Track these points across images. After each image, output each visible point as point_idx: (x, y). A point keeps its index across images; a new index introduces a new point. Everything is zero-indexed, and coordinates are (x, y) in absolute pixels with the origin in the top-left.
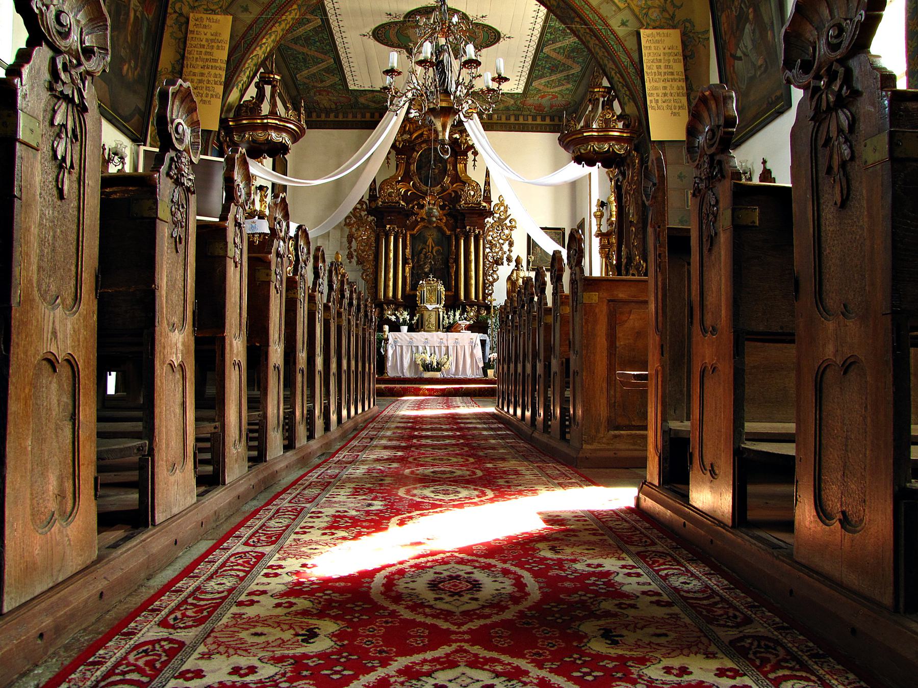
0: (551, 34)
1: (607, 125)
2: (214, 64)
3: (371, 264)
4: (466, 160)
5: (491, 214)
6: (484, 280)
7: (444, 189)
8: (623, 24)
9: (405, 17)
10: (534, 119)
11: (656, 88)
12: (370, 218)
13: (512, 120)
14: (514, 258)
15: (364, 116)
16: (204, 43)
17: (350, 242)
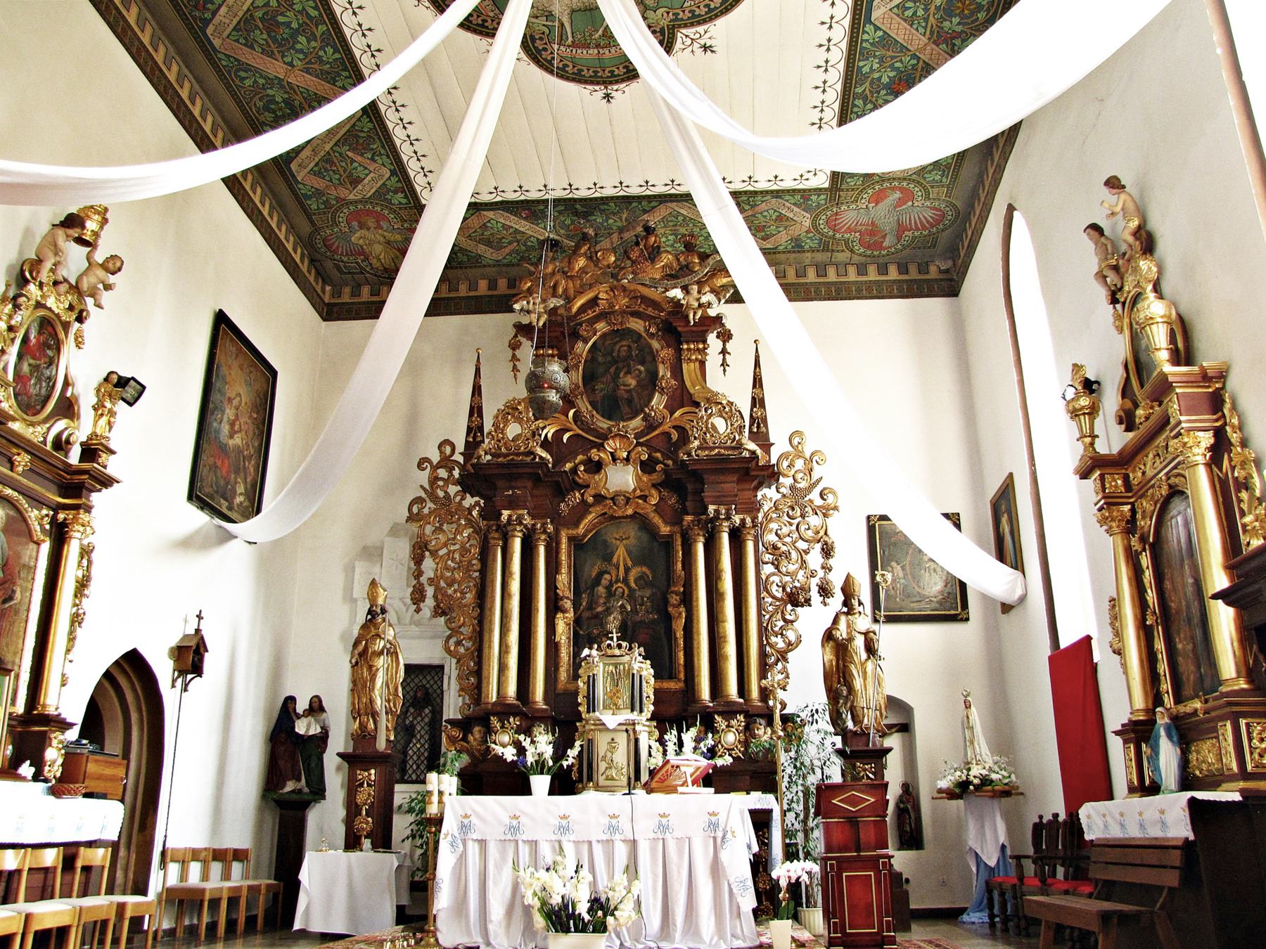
1: (455, 591)
3: (466, 614)
5: (771, 475)
6: (761, 647)
7: (651, 426)
10: (862, 270)
12: (469, 501)
13: (811, 276)
15: (473, 286)
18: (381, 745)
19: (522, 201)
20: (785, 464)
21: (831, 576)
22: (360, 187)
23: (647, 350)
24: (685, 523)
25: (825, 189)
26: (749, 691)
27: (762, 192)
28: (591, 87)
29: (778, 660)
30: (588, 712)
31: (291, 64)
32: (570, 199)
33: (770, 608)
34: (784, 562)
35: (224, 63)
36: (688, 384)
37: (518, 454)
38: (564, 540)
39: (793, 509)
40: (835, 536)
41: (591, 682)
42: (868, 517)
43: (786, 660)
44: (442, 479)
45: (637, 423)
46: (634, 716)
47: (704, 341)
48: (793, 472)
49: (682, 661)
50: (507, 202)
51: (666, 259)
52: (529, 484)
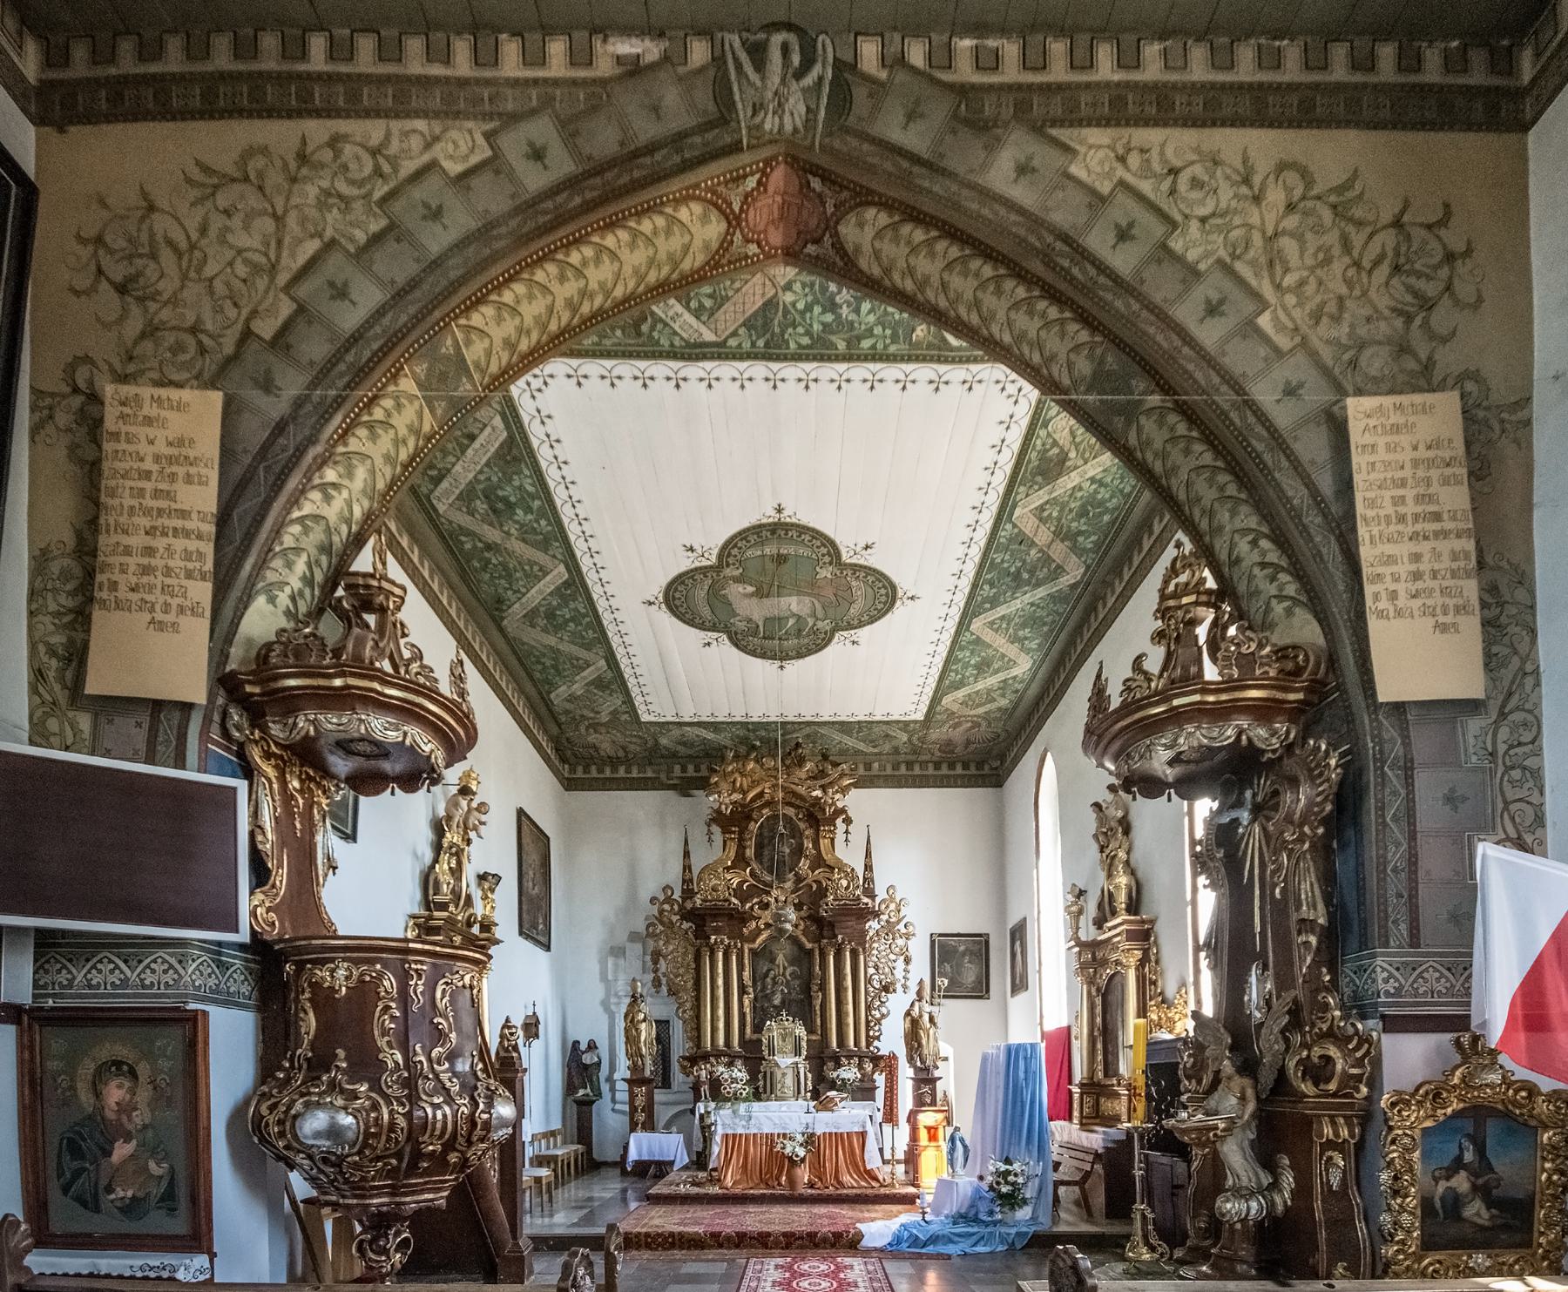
0: (992, 585)
2: (179, 523)
8: (1290, 391)
9: (720, 556)
11: (1390, 560)
12: (686, 925)
13: (903, 770)
16: (148, 465)
17: (655, 962)
18: (647, 1073)
40: (912, 952)
41: (615, 345)
51: (809, 765)
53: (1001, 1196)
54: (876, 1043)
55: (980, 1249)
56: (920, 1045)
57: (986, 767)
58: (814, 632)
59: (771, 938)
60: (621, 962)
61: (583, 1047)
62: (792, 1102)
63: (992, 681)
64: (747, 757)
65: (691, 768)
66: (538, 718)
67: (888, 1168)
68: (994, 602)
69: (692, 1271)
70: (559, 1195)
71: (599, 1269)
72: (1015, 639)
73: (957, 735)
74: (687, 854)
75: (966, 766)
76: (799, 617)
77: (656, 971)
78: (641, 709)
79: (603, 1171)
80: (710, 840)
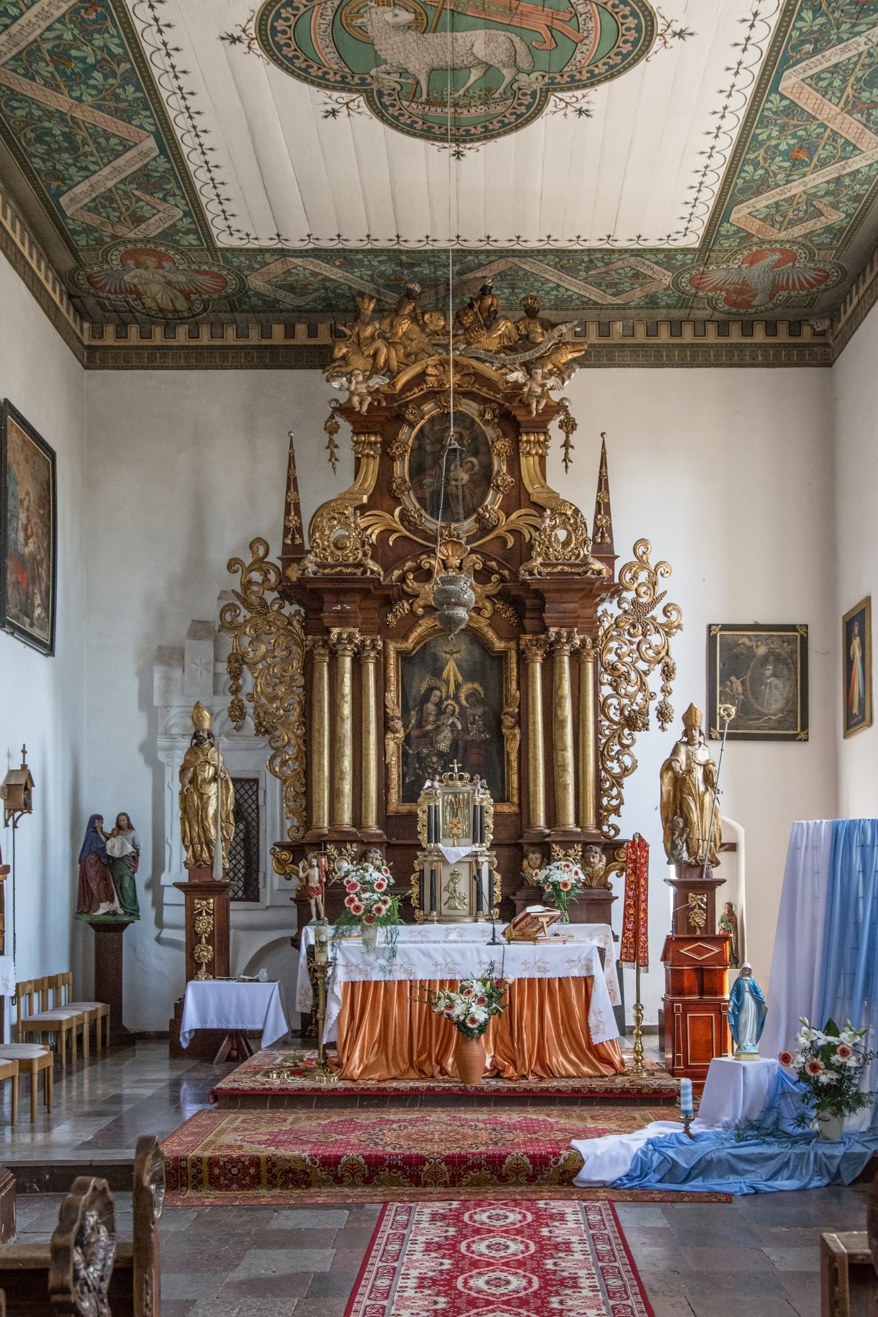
1: (278, 709)
4: (543, 445)
5: (616, 591)
7: (485, 528)
12: (289, 609)
13: (664, 336)
14: (678, 712)
17: (236, 675)
18: (218, 874)
19: (338, 250)
20: (628, 576)
21: (670, 700)
22: (143, 226)
23: (480, 439)
24: (522, 642)
25: (694, 249)
26: (585, 817)
27: (620, 251)
28: (440, 144)
29: (613, 786)
30: (429, 841)
31: (79, 100)
32: (395, 251)
33: (607, 732)
34: (624, 685)
35: (71, 227)
36: (526, 481)
37: (347, 566)
38: (392, 654)
39: (634, 627)
41: (432, 813)
42: (710, 627)
43: (621, 786)
44: (257, 583)
45: (468, 525)
46: (476, 848)
47: (545, 433)
48: (636, 585)
49: (515, 784)
50: (320, 250)
51: (504, 327)
52: (358, 598)
53: (820, 1090)
54: (613, 819)
55: (782, 1183)
56: (688, 823)
57: (806, 330)
58: (514, 92)
59: (433, 631)
60: (177, 674)
61: (108, 826)
62: (468, 925)
63: (816, 180)
64: (396, 312)
65: (301, 329)
66: (39, 240)
67: (629, 1044)
68: (821, 41)
69: (289, 1225)
70: (65, 1093)
71: (125, 1226)
72: (852, 107)
73: (757, 274)
74: (292, 483)
75: (771, 329)
76: (489, 67)
77: (236, 691)
78: (217, 225)
79: (141, 1052)
80: (332, 445)
